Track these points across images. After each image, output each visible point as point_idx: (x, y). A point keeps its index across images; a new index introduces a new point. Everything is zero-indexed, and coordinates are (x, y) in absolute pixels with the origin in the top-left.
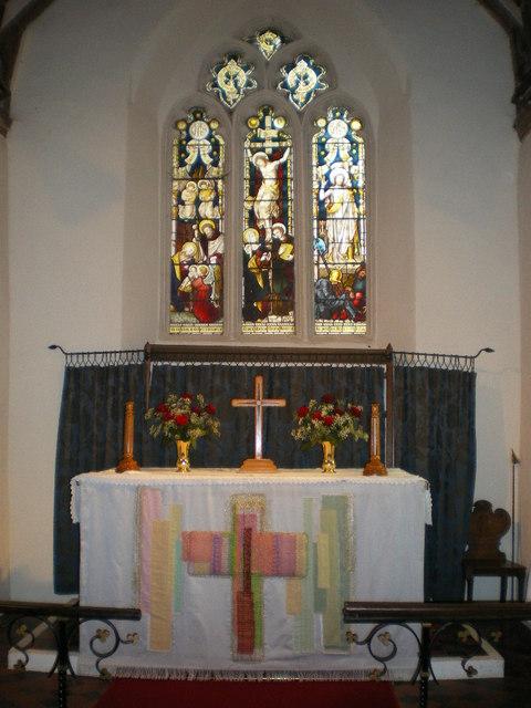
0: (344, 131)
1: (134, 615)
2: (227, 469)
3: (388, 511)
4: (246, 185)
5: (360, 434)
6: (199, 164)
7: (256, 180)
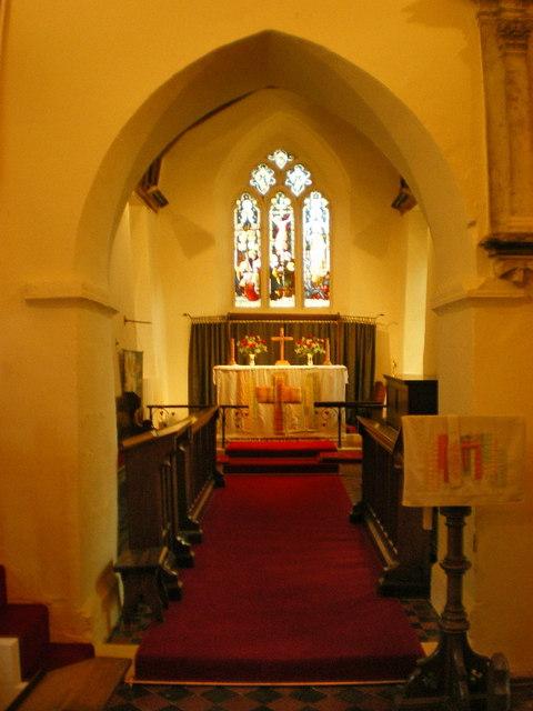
0: (320, 205)
1: (247, 407)
2: (57, 671)
3: (335, 378)
4: (271, 233)
5: (322, 351)
6: (247, 223)
7: (276, 230)
